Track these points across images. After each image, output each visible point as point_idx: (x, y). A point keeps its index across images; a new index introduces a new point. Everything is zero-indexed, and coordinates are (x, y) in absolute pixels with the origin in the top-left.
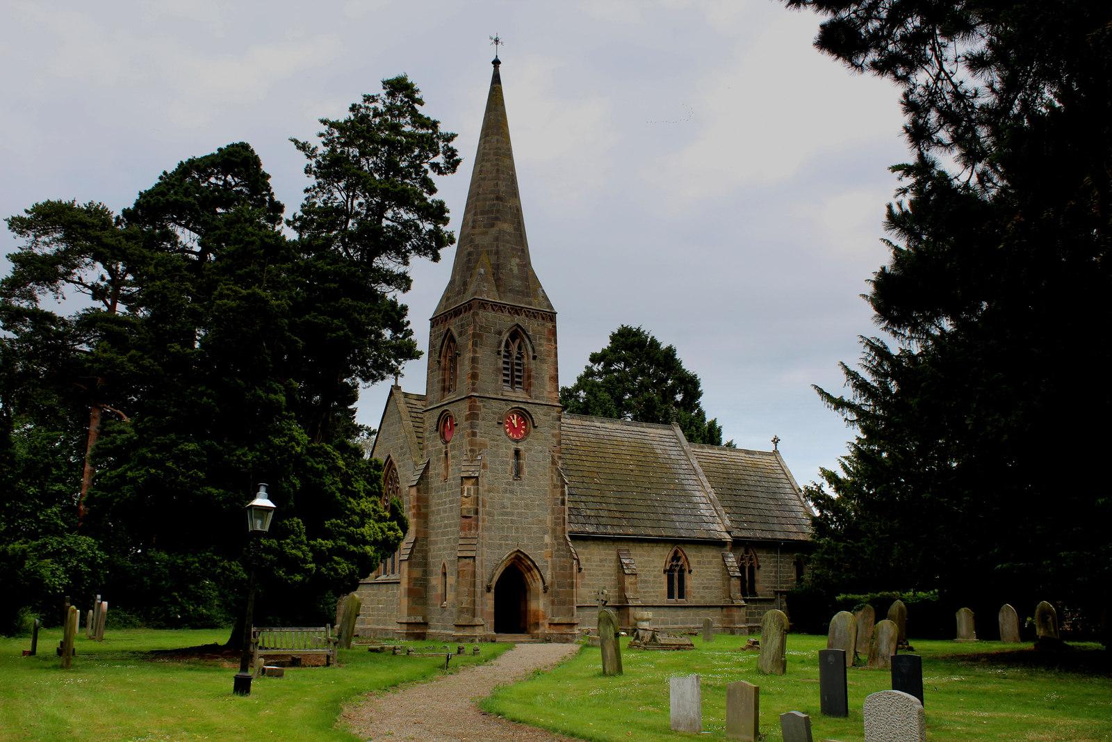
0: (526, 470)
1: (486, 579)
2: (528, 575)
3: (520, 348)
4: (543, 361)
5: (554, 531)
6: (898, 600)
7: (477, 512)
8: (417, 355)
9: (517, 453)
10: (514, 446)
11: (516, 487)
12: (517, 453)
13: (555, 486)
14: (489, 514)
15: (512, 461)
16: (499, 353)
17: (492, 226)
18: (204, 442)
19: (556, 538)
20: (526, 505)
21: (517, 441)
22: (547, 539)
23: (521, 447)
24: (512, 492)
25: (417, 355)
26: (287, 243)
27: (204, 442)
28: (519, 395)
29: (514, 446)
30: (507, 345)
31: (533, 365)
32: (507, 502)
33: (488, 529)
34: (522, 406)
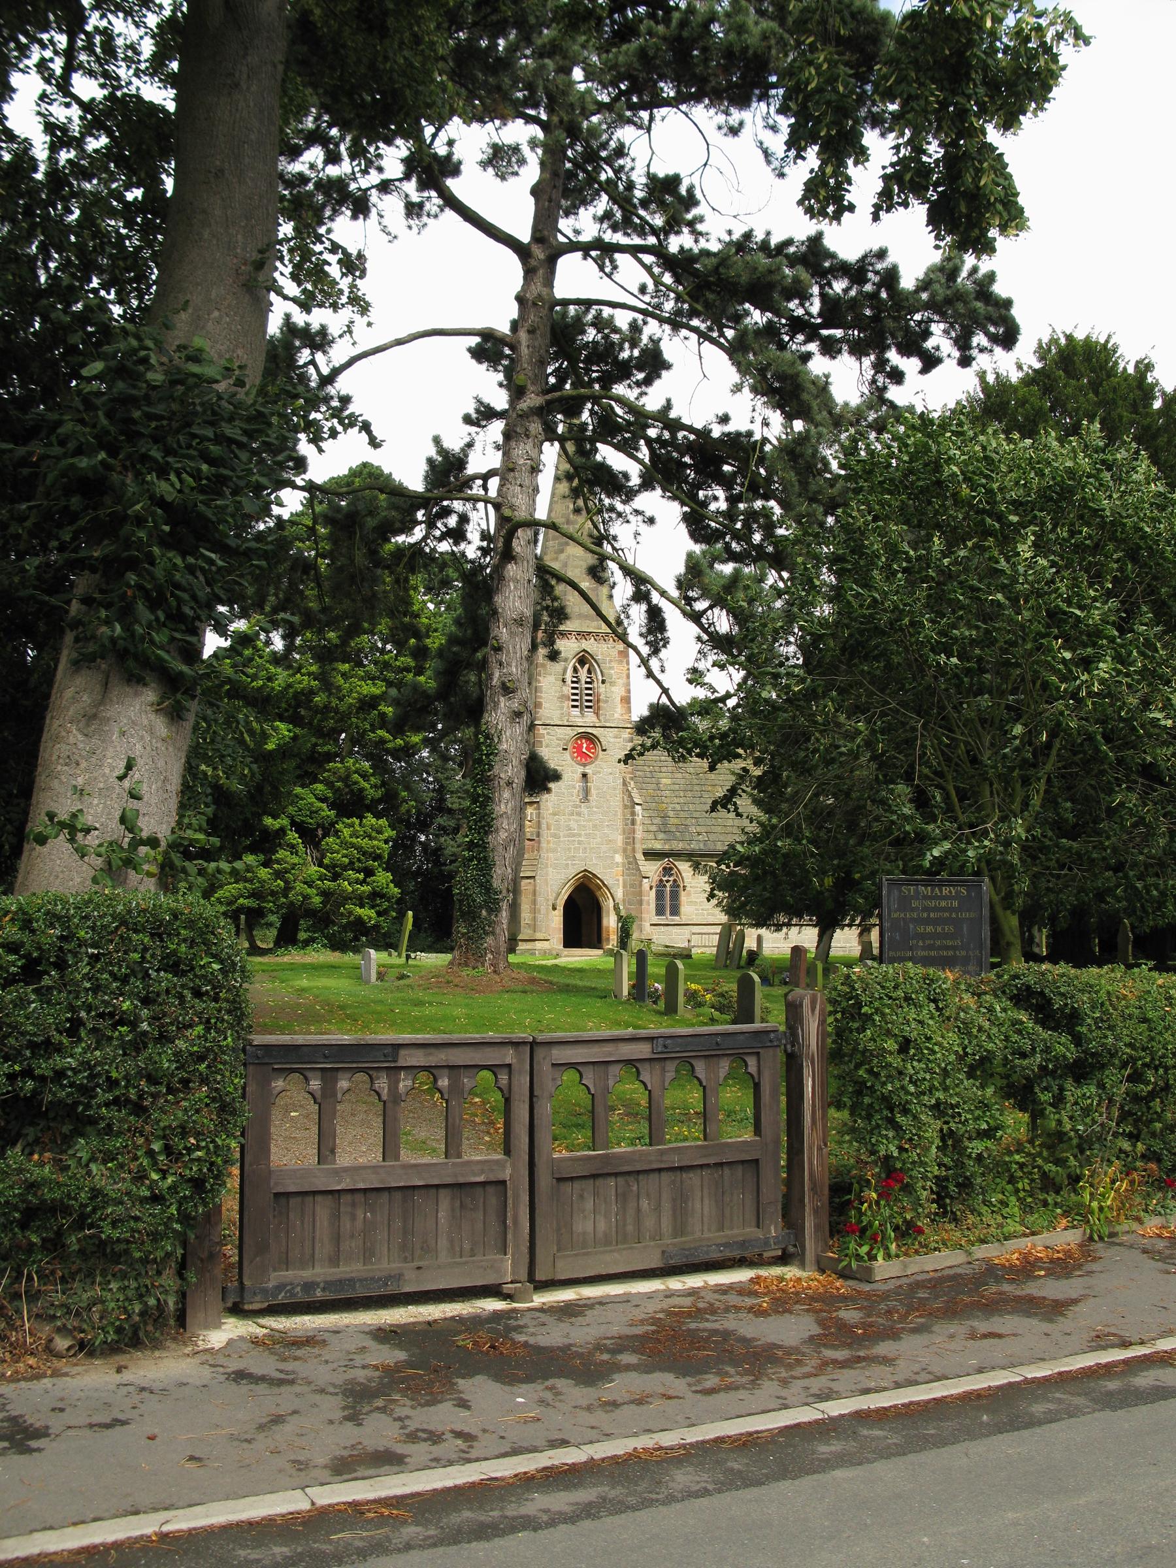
0: (593, 792)
1: (552, 897)
2: (598, 894)
3: (589, 672)
4: (612, 684)
5: (625, 850)
6: (271, 945)
7: (538, 835)
8: (819, 236)
9: (584, 775)
10: (580, 769)
11: (584, 809)
12: (584, 775)
13: (625, 807)
14: (555, 836)
15: (579, 785)
16: (564, 681)
17: (562, 551)
18: (281, 236)
19: (627, 857)
20: (595, 826)
21: (584, 765)
22: (619, 858)
23: (588, 770)
24: (579, 814)
25: (819, 236)
26: (453, 112)
27: (281, 236)
28: (590, 718)
29: (580, 769)
30: (575, 670)
31: (602, 689)
32: (573, 824)
33: (555, 851)
34: (589, 730)
